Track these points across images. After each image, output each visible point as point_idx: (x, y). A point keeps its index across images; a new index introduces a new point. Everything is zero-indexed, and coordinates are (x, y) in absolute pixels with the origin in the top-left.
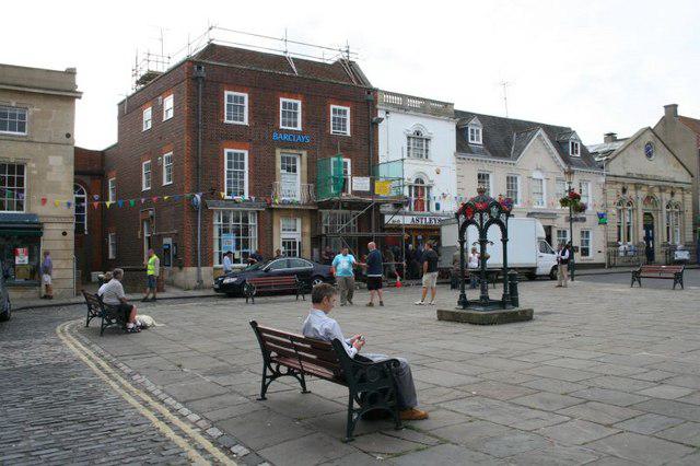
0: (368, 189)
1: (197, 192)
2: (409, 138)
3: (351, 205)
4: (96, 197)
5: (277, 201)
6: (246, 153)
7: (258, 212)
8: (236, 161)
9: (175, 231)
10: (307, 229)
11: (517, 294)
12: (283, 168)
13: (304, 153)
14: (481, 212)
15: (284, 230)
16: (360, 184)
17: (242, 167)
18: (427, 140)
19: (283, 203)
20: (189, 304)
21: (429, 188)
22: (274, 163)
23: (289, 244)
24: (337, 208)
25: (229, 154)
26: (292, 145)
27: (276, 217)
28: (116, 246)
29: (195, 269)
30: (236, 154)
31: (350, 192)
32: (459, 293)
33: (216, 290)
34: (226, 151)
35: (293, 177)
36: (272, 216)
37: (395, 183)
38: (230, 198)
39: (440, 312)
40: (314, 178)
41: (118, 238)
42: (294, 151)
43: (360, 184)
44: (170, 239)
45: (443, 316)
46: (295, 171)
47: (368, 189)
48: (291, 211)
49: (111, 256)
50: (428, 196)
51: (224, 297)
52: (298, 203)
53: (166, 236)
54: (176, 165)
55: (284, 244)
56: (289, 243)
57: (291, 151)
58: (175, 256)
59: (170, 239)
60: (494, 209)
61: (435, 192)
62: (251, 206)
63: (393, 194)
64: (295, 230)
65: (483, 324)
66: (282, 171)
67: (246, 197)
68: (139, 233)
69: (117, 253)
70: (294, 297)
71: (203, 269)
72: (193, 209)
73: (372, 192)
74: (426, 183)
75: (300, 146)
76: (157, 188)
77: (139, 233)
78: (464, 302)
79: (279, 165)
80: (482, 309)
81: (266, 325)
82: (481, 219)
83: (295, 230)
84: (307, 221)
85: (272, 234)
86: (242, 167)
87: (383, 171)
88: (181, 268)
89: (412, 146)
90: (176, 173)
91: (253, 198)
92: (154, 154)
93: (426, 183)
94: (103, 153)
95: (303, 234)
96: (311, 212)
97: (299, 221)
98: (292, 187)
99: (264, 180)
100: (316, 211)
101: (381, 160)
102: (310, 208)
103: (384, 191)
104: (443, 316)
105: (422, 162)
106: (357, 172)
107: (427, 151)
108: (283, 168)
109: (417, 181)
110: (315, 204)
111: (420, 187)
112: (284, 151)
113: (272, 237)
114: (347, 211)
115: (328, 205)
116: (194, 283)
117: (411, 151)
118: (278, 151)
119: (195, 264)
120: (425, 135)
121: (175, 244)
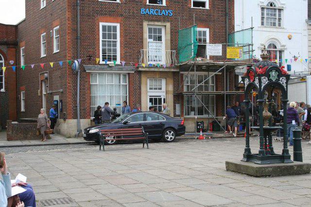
0: (221, 54)
1: (77, 58)
2: (263, 9)
3: (209, 68)
4: (12, 62)
5: (144, 65)
6: (118, 26)
7: (129, 74)
8: (109, 33)
9: (61, 90)
10: (171, 88)
11: (301, 150)
12: (150, 37)
13: (168, 25)
14: (260, 76)
15: (150, 89)
16: (214, 50)
17: (115, 37)
18: (280, 10)
19: (150, 66)
20: (69, 149)
21: (281, 52)
22: (142, 33)
23: (155, 101)
24: (192, 70)
25: (104, 27)
26: (157, 19)
27: (143, 79)
28: (25, 101)
29: (75, 121)
30: (109, 27)
31: (208, 58)
32: (244, 147)
33: (85, 138)
34: (101, 24)
35: (159, 44)
36: (140, 78)
37: (246, 49)
38: (104, 62)
39: (227, 163)
40: (175, 47)
41: (26, 95)
42: (159, 23)
43: (214, 50)
44: (58, 96)
45: (233, 168)
46: (160, 39)
47: (221, 54)
48: (156, 73)
49: (23, 109)
50: (280, 58)
51: (90, 144)
52: (162, 67)
53: (56, 94)
54: (61, 36)
55: (151, 100)
56: (156, 99)
57: (156, 23)
58: (62, 110)
59: (58, 96)
60: (274, 74)
61: (286, 56)
62: (122, 69)
63: (246, 57)
64: (161, 89)
65: (257, 177)
66: (149, 40)
67: (118, 62)
68: (39, 91)
69: (26, 107)
70: (141, 145)
71: (82, 120)
72: (74, 73)
73: (224, 57)
74: (279, 48)
75: (164, 19)
76: (51, 56)
77: (39, 91)
78: (248, 156)
79: (146, 34)
80: (259, 162)
81: (7, 162)
82: (260, 82)
83: (161, 89)
84: (171, 82)
85: (140, 92)
86: (115, 37)
87: (238, 38)
88: (65, 119)
89: (265, 16)
90: (61, 46)
91: (124, 63)
92: (48, 28)
93: (279, 48)
94: (16, 27)
95: (167, 92)
96: (176, 73)
97: (164, 82)
98: (157, 52)
99: (133, 46)
100: (178, 72)
101: (236, 29)
102: (173, 70)
103: (235, 54)
104: (233, 168)
105: (275, 30)
106: (214, 41)
107: (280, 19)
108: (150, 37)
109: (270, 46)
110: (177, 67)
111: (272, 52)
112: (152, 23)
113: (140, 94)
114: (206, 73)
115: (186, 68)
116: (75, 132)
117: (265, 20)
118: (145, 24)
119: (75, 117)
120: (278, 6)
121: (61, 101)
